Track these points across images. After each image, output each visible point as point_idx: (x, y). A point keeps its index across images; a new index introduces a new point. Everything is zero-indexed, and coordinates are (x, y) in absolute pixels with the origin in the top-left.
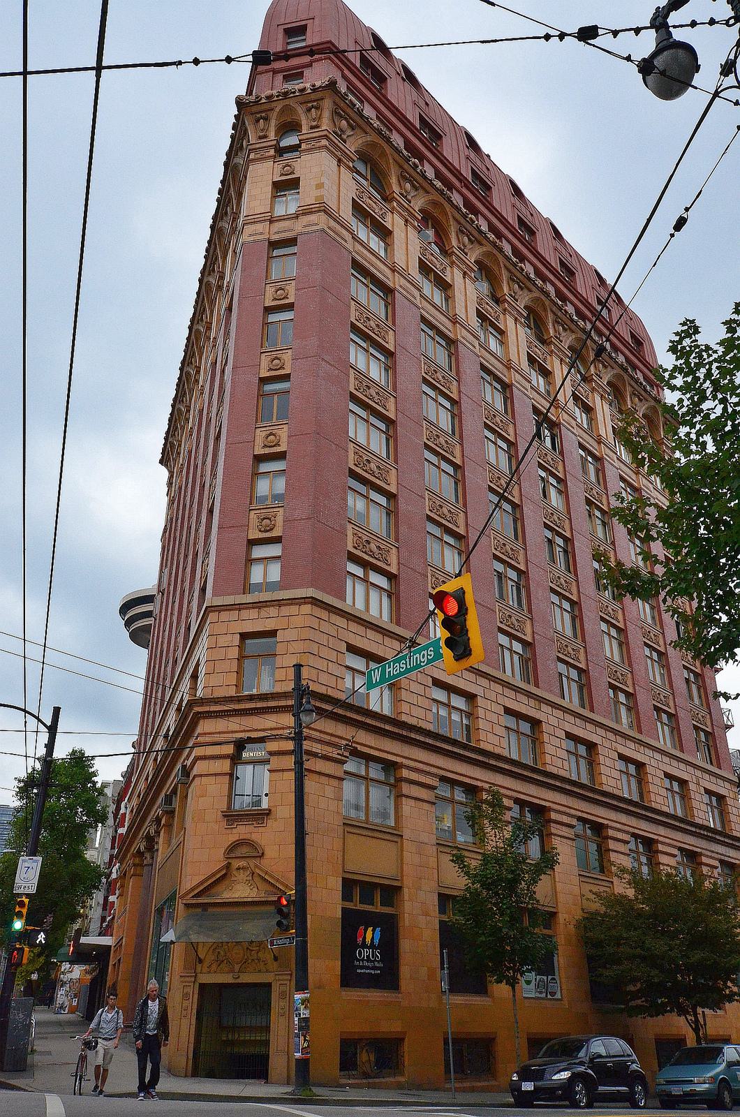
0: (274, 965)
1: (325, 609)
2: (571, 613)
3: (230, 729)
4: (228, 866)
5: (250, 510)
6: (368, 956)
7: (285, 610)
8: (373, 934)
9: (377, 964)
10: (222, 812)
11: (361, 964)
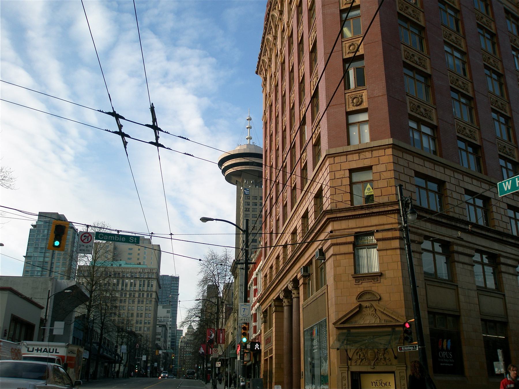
0: (395, 362)
1: (400, 150)
2: (506, 123)
3: (350, 226)
4: (360, 306)
5: (345, 94)
6: (445, 356)
7: (376, 153)
8: (447, 343)
9: (451, 361)
10: (352, 275)
11: (442, 360)
